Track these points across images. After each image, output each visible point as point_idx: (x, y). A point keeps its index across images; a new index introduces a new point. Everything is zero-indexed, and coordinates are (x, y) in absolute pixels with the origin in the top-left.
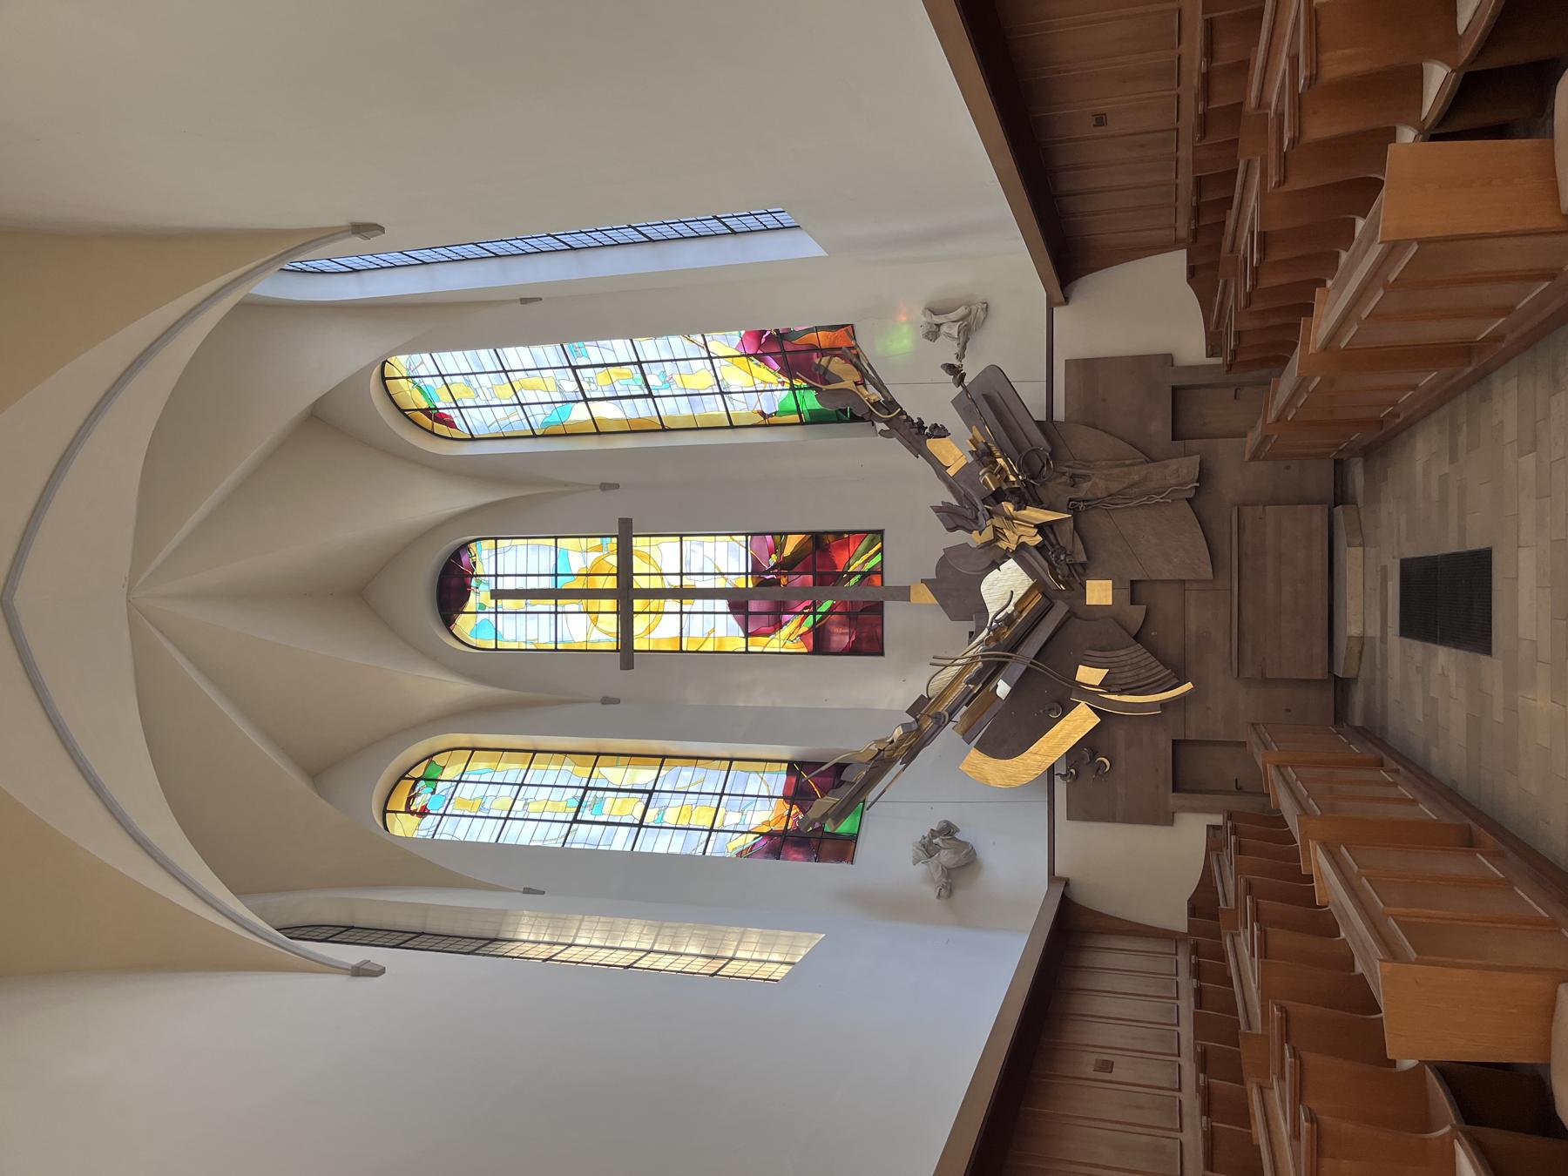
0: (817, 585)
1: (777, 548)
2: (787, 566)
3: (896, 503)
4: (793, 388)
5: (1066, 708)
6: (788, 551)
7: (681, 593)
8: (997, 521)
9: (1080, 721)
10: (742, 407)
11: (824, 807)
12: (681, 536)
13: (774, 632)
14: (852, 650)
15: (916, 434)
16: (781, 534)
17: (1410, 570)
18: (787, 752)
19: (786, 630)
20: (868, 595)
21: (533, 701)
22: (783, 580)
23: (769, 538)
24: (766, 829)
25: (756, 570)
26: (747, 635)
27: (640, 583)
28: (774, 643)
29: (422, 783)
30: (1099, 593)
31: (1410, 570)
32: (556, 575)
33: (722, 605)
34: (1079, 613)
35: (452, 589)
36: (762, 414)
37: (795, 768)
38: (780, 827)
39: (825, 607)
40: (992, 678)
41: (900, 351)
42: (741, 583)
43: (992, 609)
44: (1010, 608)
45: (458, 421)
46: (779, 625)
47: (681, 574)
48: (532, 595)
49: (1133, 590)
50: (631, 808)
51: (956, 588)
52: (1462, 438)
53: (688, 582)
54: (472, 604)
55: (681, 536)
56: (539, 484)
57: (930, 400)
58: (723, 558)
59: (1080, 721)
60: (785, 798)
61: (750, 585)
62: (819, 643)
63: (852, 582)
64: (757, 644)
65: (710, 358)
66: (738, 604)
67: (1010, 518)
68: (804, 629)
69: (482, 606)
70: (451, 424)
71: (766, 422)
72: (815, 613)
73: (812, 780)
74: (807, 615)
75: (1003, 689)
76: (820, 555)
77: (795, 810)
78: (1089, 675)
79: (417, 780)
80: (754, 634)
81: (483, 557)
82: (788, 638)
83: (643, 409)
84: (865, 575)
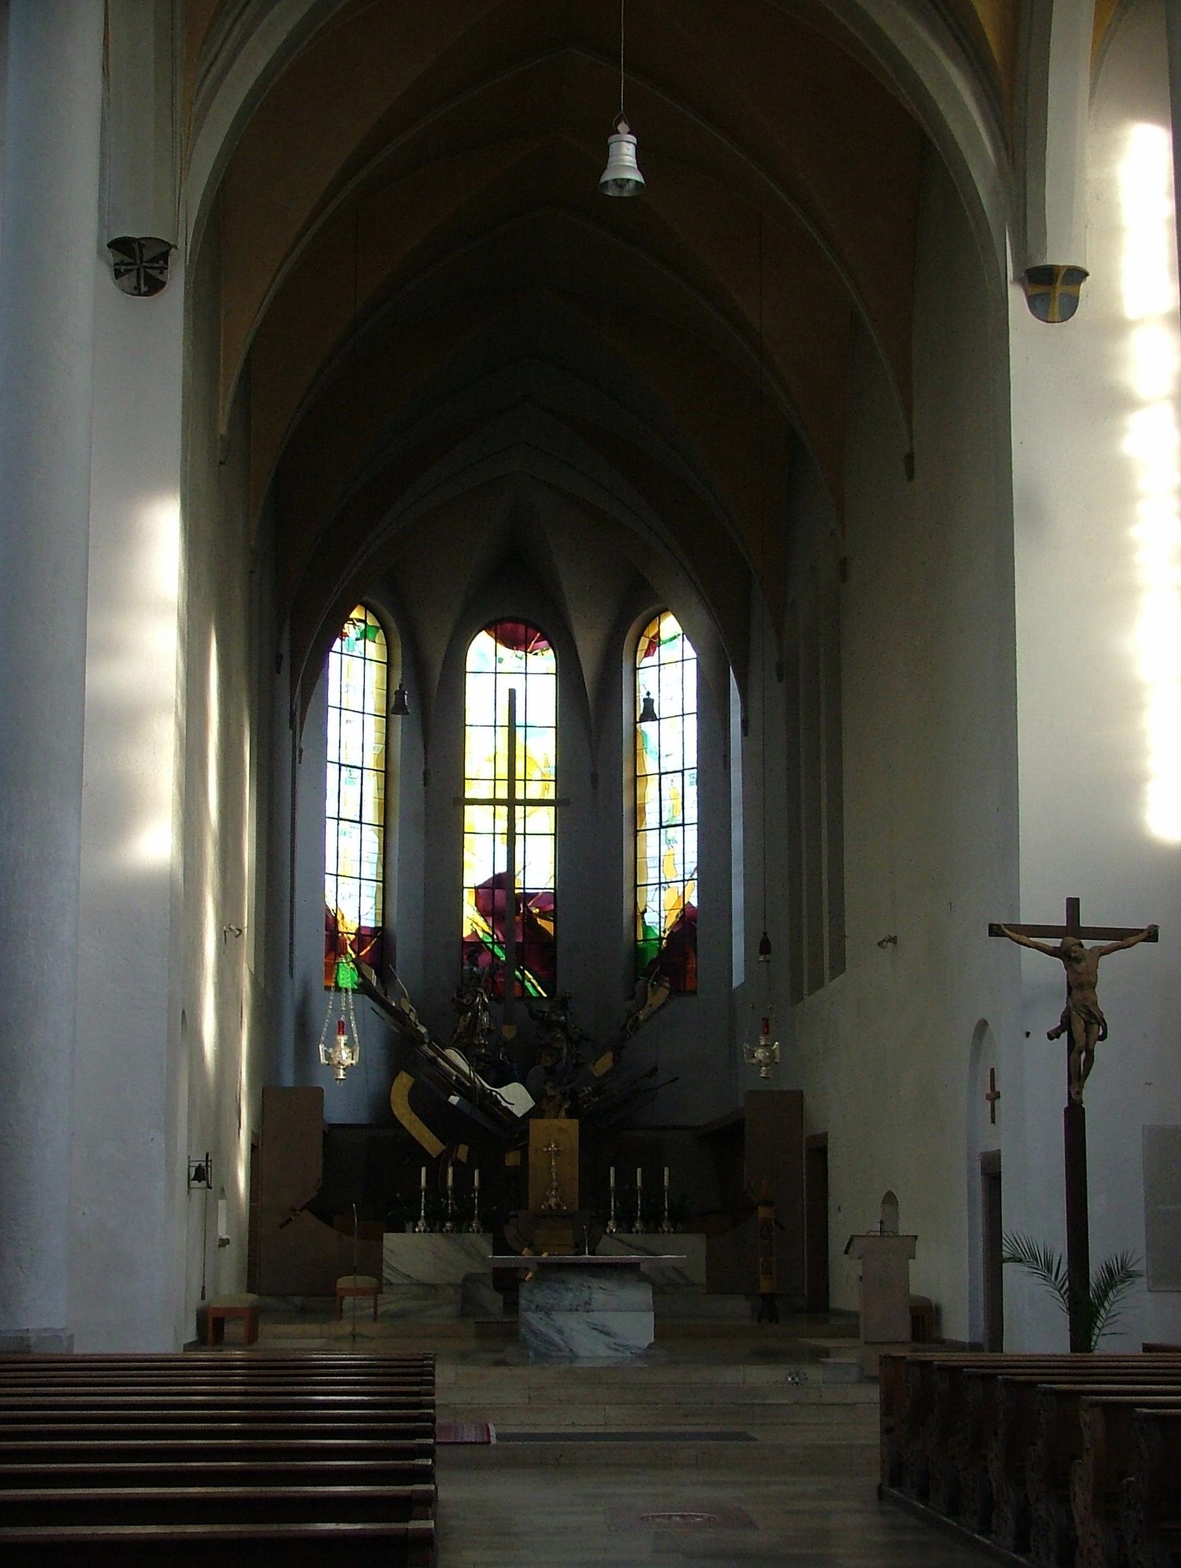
1: (543, 915)
2: (530, 918)
4: (660, 939)
5: (443, 1140)
6: (539, 921)
7: (511, 835)
8: (559, 1097)
9: (431, 1143)
12: (555, 835)
13: (479, 910)
16: (555, 916)
19: (480, 920)
21: (425, 709)
22: (518, 918)
23: (552, 907)
24: (339, 918)
25: (527, 897)
26: (476, 888)
27: (519, 810)
29: (362, 626)
32: (525, 780)
33: (502, 868)
36: (645, 911)
38: (341, 928)
39: (498, 951)
40: (460, 1093)
42: (518, 883)
43: (503, 1091)
44: (504, 1104)
45: (647, 661)
46: (483, 913)
47: (525, 834)
48: (509, 689)
50: (350, 812)
53: (519, 840)
54: (503, 651)
55: (555, 835)
56: (596, 726)
59: (431, 1143)
60: (360, 928)
61: (517, 891)
63: (517, 973)
64: (469, 898)
65: (684, 881)
66: (502, 882)
67: (560, 1106)
68: (481, 934)
69: (501, 661)
70: (648, 654)
72: (493, 943)
74: (492, 937)
75: (454, 1099)
77: (352, 937)
79: (364, 622)
80: (477, 893)
82: (473, 922)
83: (651, 820)
84: (522, 983)
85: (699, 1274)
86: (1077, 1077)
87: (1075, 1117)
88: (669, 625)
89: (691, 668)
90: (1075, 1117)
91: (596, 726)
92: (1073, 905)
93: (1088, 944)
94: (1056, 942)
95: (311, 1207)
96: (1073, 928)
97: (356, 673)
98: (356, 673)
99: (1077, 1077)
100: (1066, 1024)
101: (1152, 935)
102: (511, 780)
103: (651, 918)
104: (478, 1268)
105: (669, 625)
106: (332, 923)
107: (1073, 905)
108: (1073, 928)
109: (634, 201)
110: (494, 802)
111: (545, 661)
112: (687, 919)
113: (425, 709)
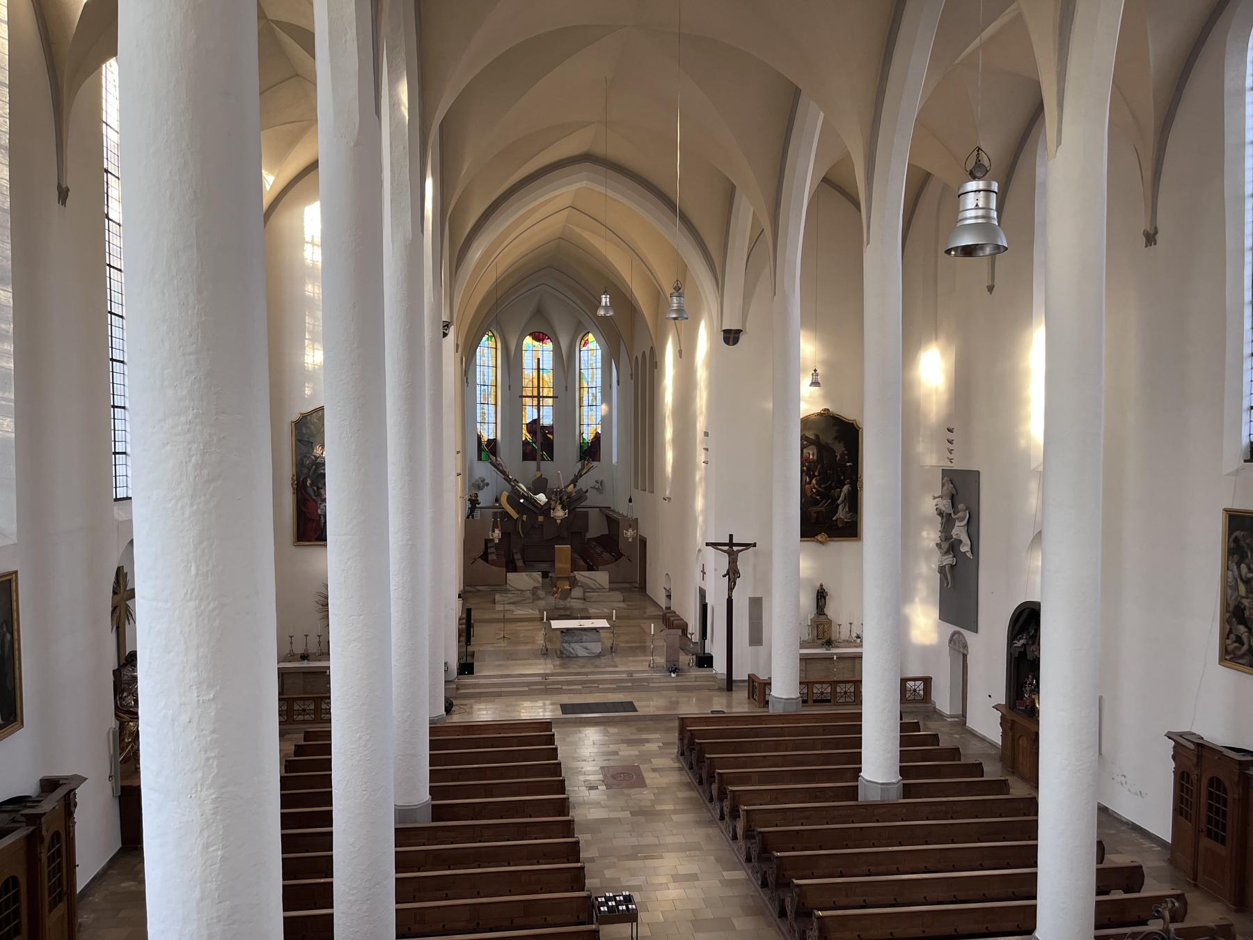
0: (541, 442)
3: (562, 468)
7: (538, 406)
9: (515, 515)
10: (585, 428)
11: (489, 449)
14: (524, 454)
15: (574, 482)
17: (981, 764)
18: (499, 438)
20: (539, 457)
21: (511, 363)
28: (525, 431)
30: (541, 518)
31: (981, 764)
33: (536, 417)
34: (537, 515)
35: (539, 337)
37: (495, 440)
41: (596, 472)
48: (537, 355)
49: (541, 525)
51: (540, 485)
52: (692, 853)
54: (535, 343)
56: (565, 365)
57: (583, 483)
58: (547, 420)
59: (515, 515)
62: (526, 443)
64: (524, 427)
66: (535, 422)
71: (581, 434)
73: (492, 446)
76: (548, 446)
78: (525, 517)
81: (549, 346)
82: (526, 435)
83: (585, 403)
85: (606, 585)
86: (731, 589)
87: (730, 602)
88: (591, 337)
89: (599, 353)
90: (730, 602)
91: (565, 365)
92: (731, 536)
93: (735, 548)
94: (726, 548)
95: (481, 557)
96: (731, 544)
97: (487, 353)
98: (487, 353)
99: (731, 589)
100: (728, 573)
101: (755, 545)
102: (538, 406)
103: (585, 436)
104: (537, 585)
105: (591, 337)
106: (479, 438)
107: (731, 536)
108: (731, 544)
109: (605, 293)
110: (533, 397)
111: (549, 346)
112: (597, 437)
113: (511, 363)
